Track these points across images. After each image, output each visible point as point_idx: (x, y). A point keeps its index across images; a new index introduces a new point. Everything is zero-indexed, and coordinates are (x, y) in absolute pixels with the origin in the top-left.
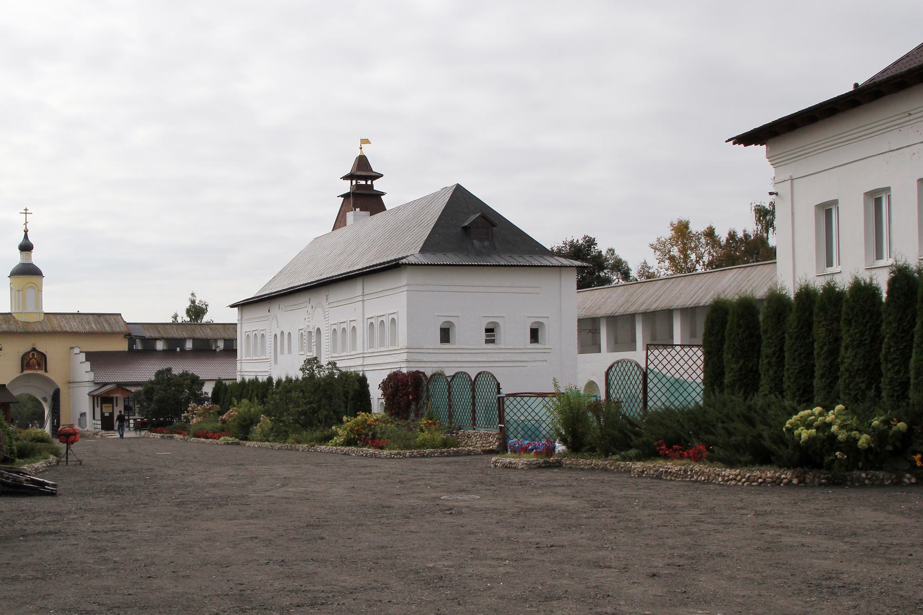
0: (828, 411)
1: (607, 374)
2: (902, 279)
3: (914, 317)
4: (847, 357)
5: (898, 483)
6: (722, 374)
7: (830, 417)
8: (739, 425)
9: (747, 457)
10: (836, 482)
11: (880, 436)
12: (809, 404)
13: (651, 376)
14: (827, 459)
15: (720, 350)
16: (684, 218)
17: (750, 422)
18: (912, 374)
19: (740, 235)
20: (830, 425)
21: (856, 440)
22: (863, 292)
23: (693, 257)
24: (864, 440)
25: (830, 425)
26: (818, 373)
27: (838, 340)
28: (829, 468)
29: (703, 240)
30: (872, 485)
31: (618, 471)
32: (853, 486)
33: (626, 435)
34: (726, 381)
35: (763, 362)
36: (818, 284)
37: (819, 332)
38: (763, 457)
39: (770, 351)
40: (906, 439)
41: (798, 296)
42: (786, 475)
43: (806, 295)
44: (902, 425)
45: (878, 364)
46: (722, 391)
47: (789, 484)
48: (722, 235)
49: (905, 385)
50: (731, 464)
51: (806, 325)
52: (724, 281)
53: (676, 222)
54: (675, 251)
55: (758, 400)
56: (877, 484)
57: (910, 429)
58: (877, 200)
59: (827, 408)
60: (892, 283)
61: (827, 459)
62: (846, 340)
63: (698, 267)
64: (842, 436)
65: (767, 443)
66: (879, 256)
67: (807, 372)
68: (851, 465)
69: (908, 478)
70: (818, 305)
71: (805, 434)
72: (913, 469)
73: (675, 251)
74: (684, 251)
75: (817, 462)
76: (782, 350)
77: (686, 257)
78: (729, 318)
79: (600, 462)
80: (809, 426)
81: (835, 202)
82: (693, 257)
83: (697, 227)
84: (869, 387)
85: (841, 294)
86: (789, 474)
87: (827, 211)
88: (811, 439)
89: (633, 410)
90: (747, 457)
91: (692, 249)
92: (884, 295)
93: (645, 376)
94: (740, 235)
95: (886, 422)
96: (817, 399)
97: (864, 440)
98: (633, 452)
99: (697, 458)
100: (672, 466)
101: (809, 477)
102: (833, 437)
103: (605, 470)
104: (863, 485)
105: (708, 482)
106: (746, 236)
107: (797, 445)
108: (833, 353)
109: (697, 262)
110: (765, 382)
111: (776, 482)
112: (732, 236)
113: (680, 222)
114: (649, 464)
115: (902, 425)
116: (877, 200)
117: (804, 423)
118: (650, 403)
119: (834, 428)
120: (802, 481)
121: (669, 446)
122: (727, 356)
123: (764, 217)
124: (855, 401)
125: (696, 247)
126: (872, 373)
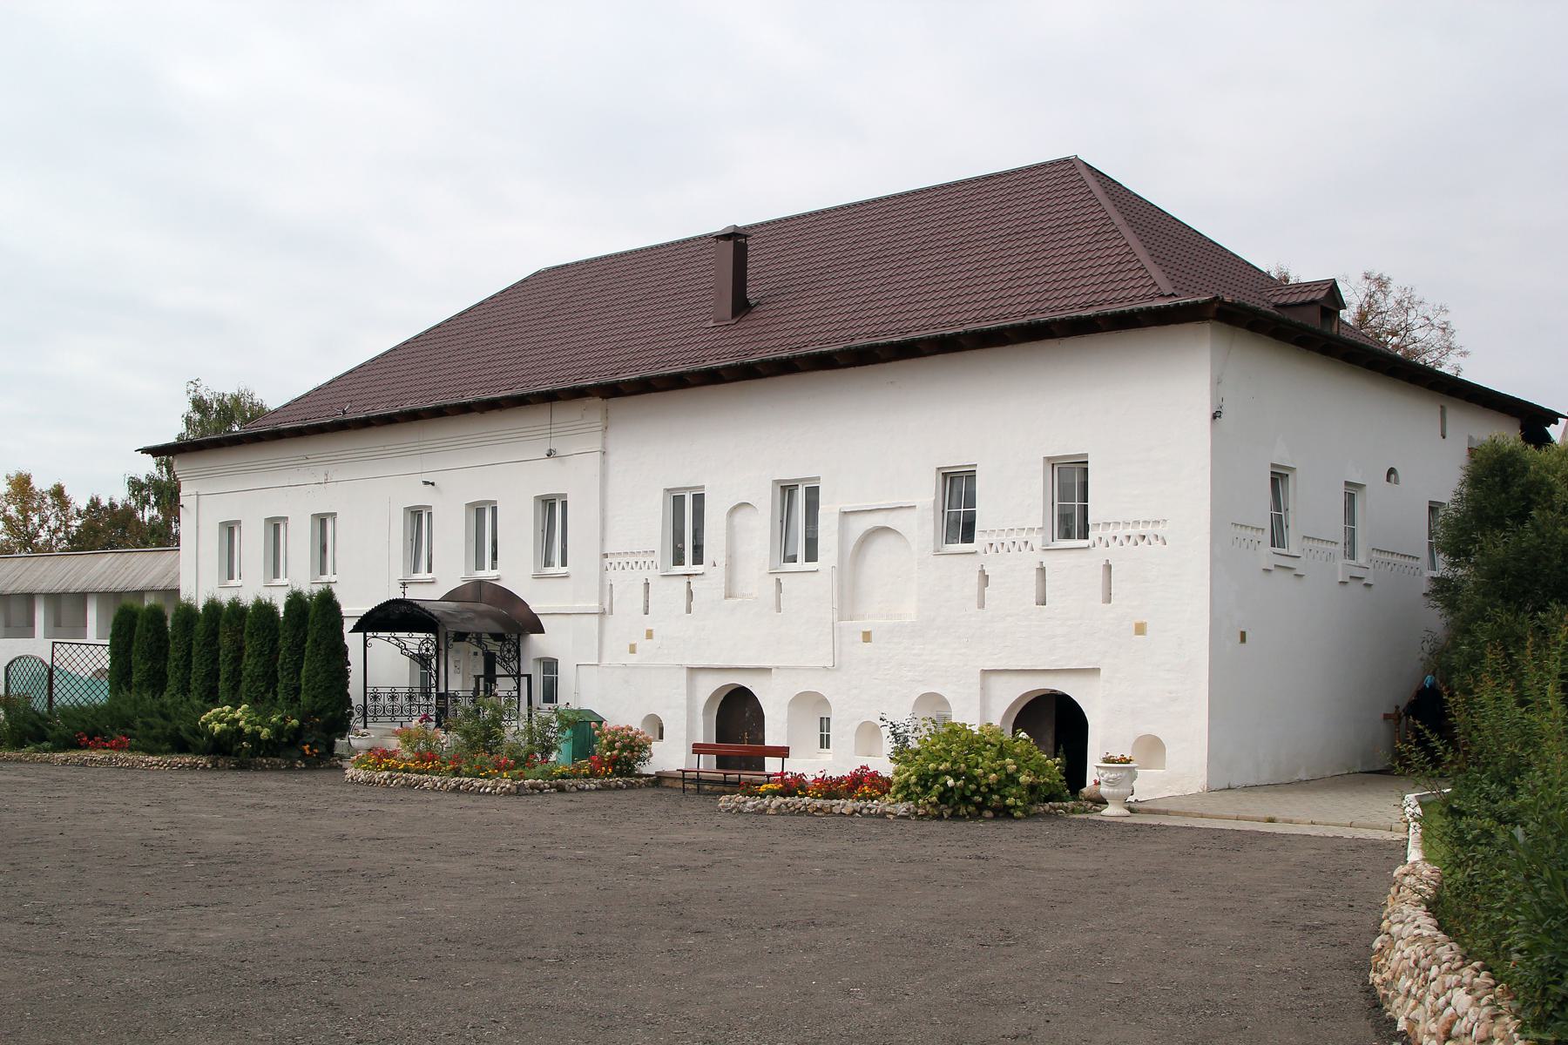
0: (1523, 523)
1: (7, 669)
2: (295, 600)
3: (306, 635)
4: (249, 665)
5: (291, 768)
6: (130, 673)
7: (238, 714)
8: (160, 721)
9: (167, 746)
10: (242, 767)
11: (278, 731)
12: (215, 702)
13: (56, 673)
14: (236, 748)
15: (128, 650)
16: (26, 471)
17: (165, 717)
18: (303, 681)
19: (105, 503)
20: (238, 720)
21: (259, 733)
22: (264, 610)
23: (36, 520)
24: (265, 733)
25: (238, 720)
26: (222, 677)
27: (241, 649)
28: (237, 755)
29: (49, 500)
30: (271, 769)
31: (34, 761)
32: (256, 770)
33: (38, 727)
34: (134, 680)
35: (171, 665)
36: (225, 598)
37: (225, 641)
38: (181, 747)
39: (177, 655)
40: (298, 733)
41: (206, 608)
42: (203, 760)
43: (213, 607)
44: (295, 722)
45: (275, 672)
46: (129, 690)
47: (205, 767)
48: (80, 501)
49: (297, 690)
50: (151, 753)
51: (214, 634)
52: (97, 567)
53: (13, 474)
54: (12, 511)
55: (167, 698)
56: (275, 768)
57: (301, 725)
58: (275, 526)
59: (236, 707)
60: (288, 605)
61: (236, 748)
62: (248, 650)
63: (41, 532)
64: (248, 729)
65: (185, 735)
66: (276, 575)
67: (213, 675)
68: (254, 753)
69: (299, 764)
70: (224, 620)
71: (218, 727)
72: (303, 756)
73: (12, 511)
74: (24, 511)
75: (228, 751)
76: (189, 654)
77: (27, 519)
78: (139, 622)
79: (13, 754)
80: (220, 721)
81: (239, 522)
82: (36, 520)
83: (41, 484)
84: (267, 691)
85: (245, 609)
86: (204, 760)
87: (230, 528)
88: (223, 732)
89: (40, 704)
90: (167, 746)
91: (34, 510)
92: (282, 610)
93: (51, 672)
94: (105, 503)
95: (283, 719)
96: (222, 699)
97: (265, 733)
98: (46, 744)
99: (119, 747)
100: (98, 755)
101: (221, 762)
102: (241, 730)
103: (19, 761)
104: (264, 769)
105: (132, 767)
106: (112, 505)
107: (210, 737)
108: (237, 659)
109: (41, 526)
110: (172, 684)
111: (193, 767)
112: (95, 504)
113: (20, 476)
114: (73, 754)
115: (295, 722)
116: (275, 526)
117: (217, 719)
118: (56, 699)
119: (242, 723)
120: (215, 766)
121: (91, 738)
122: (135, 658)
123: (140, 491)
124: (255, 702)
125: (40, 507)
126: (271, 679)
